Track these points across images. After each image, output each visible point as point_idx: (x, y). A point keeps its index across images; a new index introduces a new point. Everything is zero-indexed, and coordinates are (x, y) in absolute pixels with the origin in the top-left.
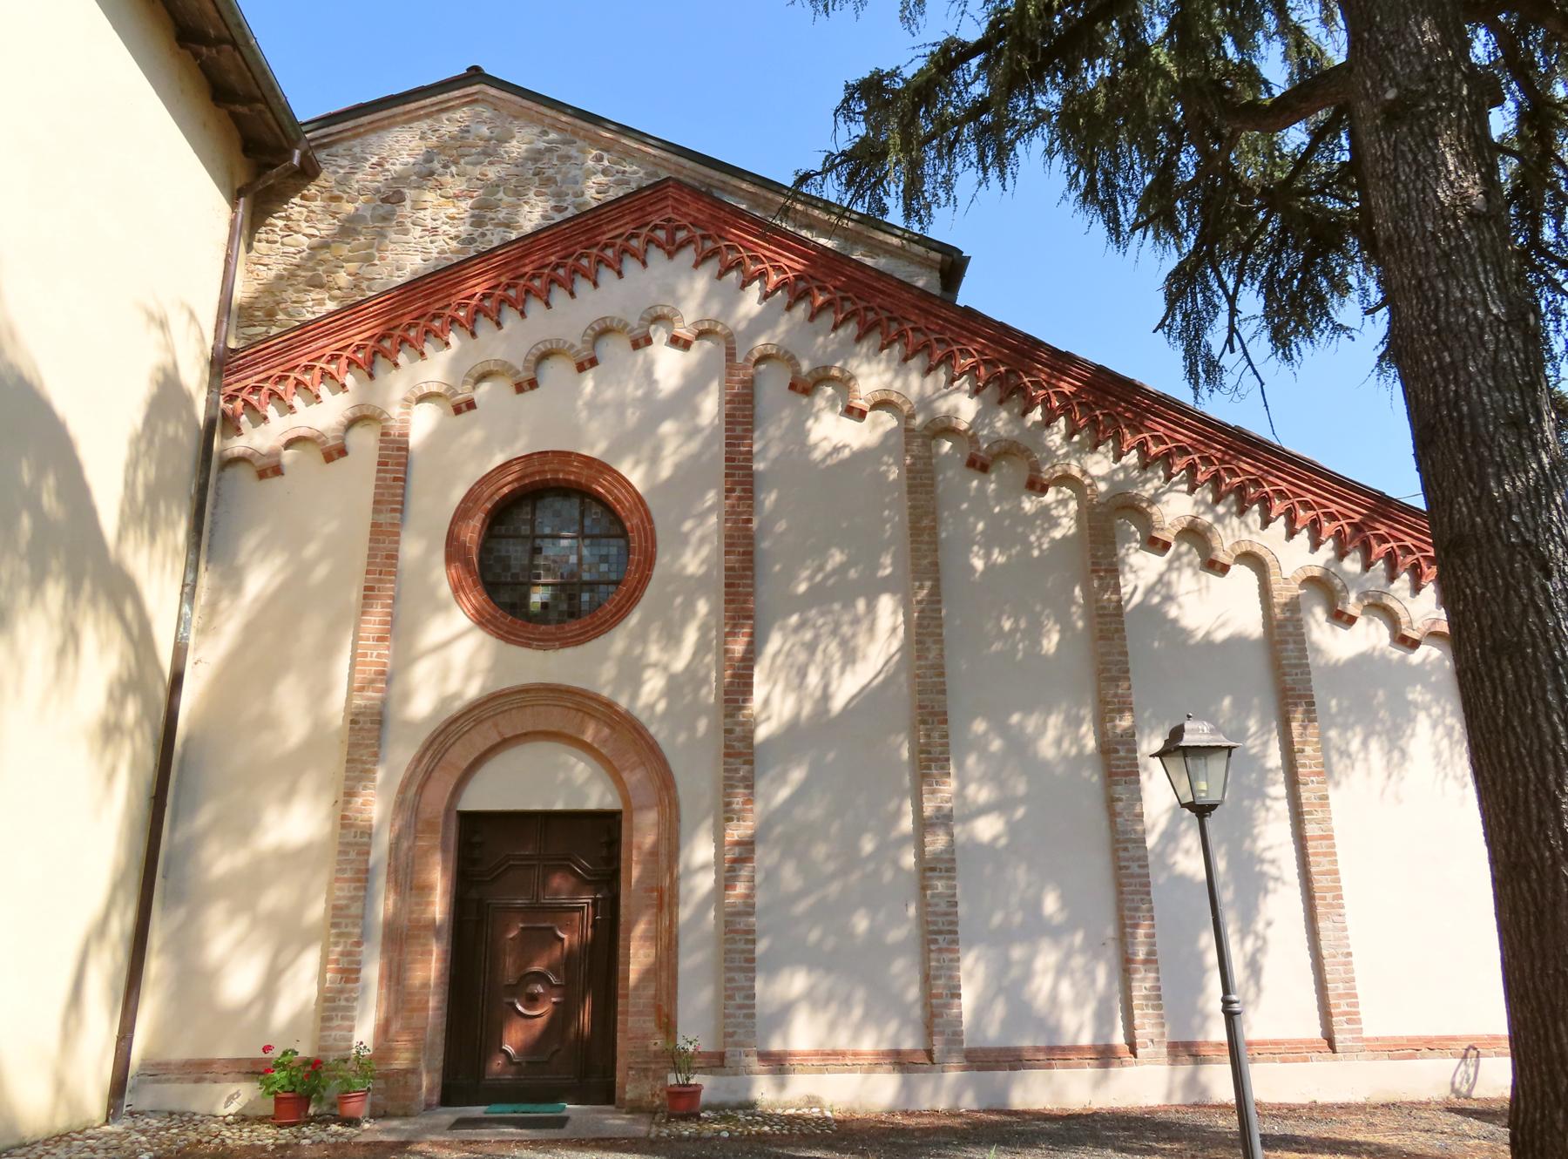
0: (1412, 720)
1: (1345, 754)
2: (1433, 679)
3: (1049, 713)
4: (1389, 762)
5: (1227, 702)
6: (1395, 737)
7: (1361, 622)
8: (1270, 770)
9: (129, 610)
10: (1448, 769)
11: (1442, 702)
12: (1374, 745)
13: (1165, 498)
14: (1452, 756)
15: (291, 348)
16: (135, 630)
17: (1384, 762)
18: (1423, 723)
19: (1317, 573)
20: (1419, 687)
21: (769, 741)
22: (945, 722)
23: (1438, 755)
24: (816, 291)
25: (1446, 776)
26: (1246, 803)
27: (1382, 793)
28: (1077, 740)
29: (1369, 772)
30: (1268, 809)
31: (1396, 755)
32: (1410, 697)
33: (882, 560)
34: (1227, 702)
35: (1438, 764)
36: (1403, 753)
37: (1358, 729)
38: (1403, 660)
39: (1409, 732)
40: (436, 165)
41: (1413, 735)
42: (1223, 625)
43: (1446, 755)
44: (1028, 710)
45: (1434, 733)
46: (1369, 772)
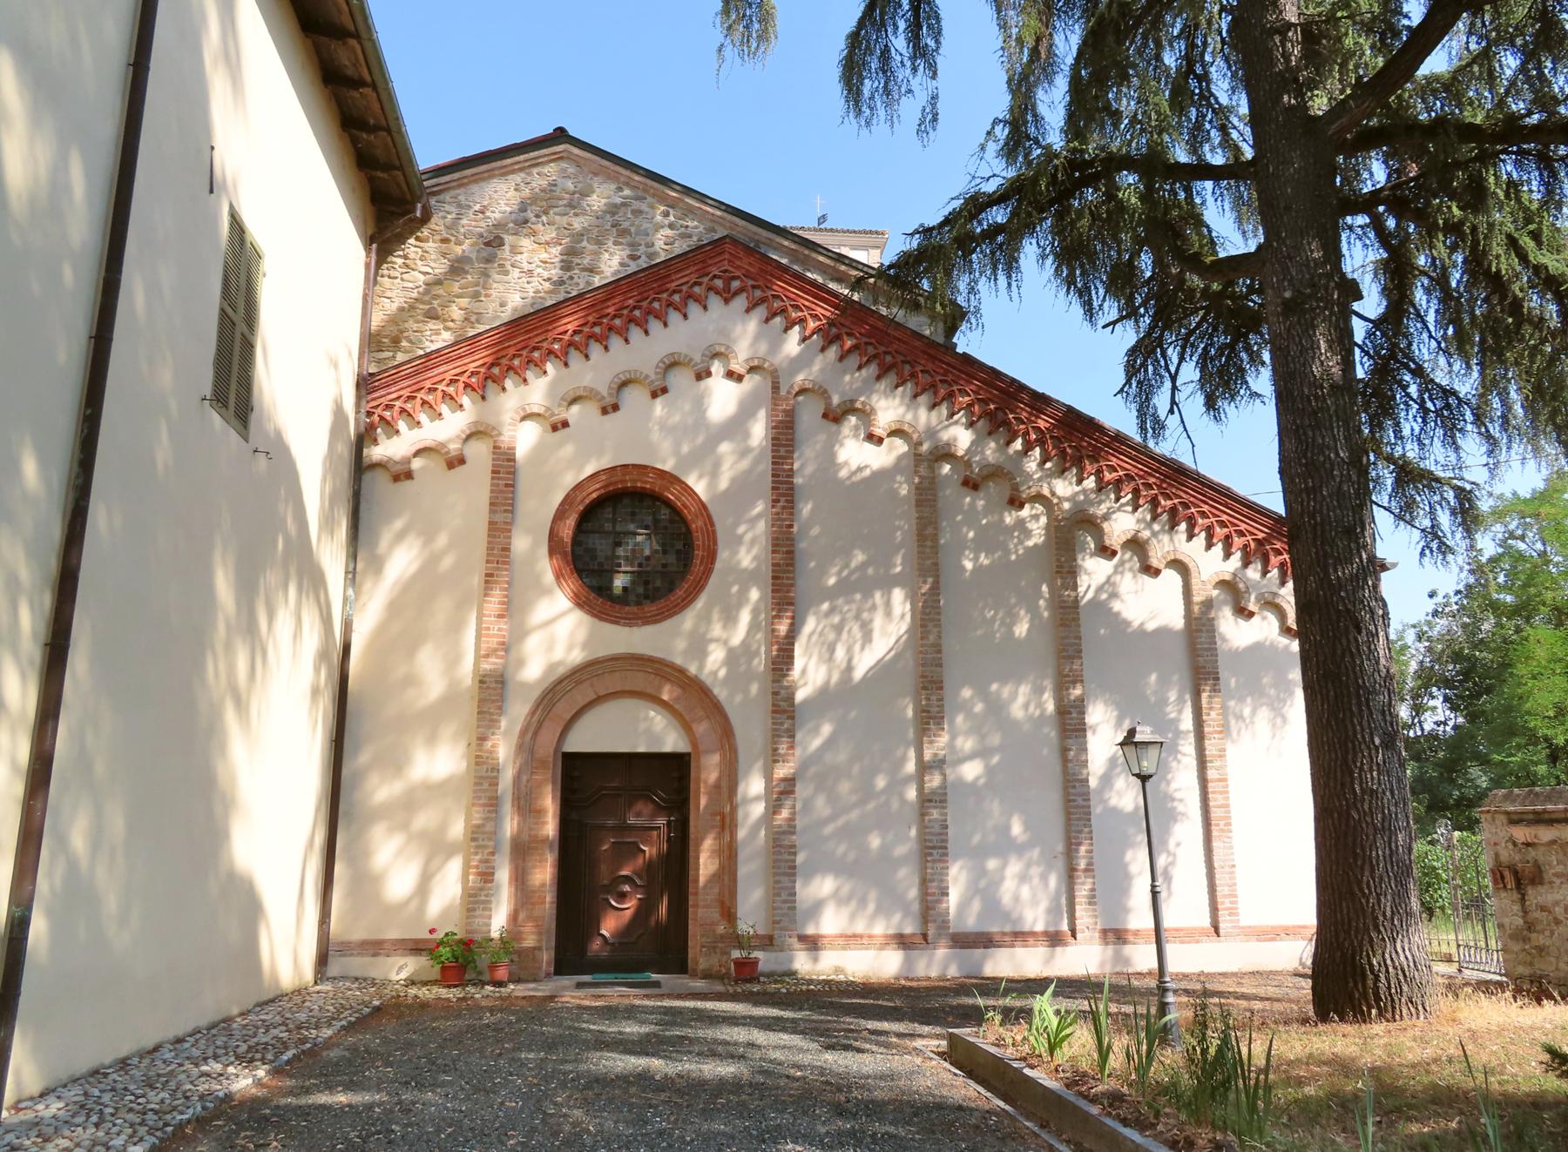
1: (1240, 717)
3: (1019, 684)
5: (1153, 677)
13: (1114, 516)
19: (1228, 577)
22: (941, 688)
28: (1040, 705)
34: (1153, 677)
36: (1284, 719)
41: (1291, 706)
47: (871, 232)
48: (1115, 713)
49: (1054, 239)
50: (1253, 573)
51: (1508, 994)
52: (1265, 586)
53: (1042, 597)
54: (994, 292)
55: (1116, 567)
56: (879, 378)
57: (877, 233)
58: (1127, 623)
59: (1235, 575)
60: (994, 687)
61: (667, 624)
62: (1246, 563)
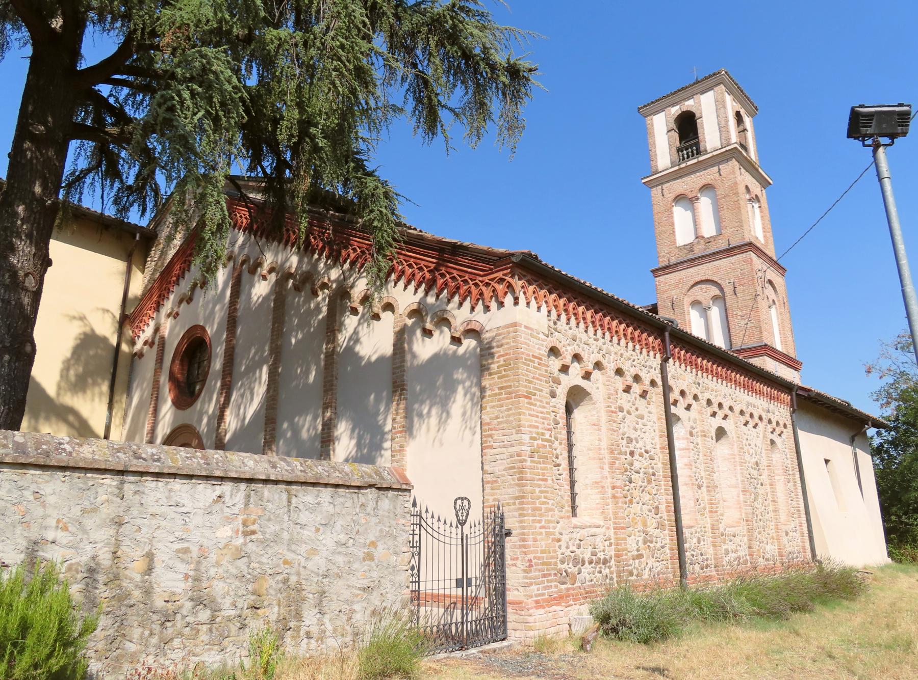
0: (454, 391)
1: (420, 415)
2: (469, 362)
3: (307, 415)
4: (440, 420)
5: (372, 397)
6: (444, 404)
7: (436, 334)
8: (386, 433)
9: (71, 418)
10: (468, 423)
11: (472, 377)
12: (434, 411)
13: (357, 283)
14: (471, 413)
15: (141, 310)
16: (77, 424)
17: (437, 421)
18: (460, 390)
19: (415, 307)
20: (460, 370)
21: (229, 441)
22: (275, 423)
23: (464, 414)
24: (789, 612)
25: (466, 427)
26: (374, 453)
27: (434, 441)
28: (315, 428)
29: (428, 430)
30: (382, 456)
31: (444, 415)
32: (455, 376)
33: (455, 376)
34: (372, 397)
35: (463, 420)
36: (448, 413)
37: (428, 402)
38: (455, 352)
39: (452, 399)
40: (641, 471)
41: (454, 402)
42: (375, 352)
43: (469, 413)
44: (300, 415)
45: (465, 399)
46: (428, 430)
47: (710, 76)
48: (351, 426)
49: (273, 162)
50: (431, 300)
51: (106, 329)
52: (438, 306)
53: (322, 352)
54: (140, 213)
55: (360, 320)
56: (279, 245)
57: (714, 74)
58: (361, 358)
59: (419, 303)
60: (296, 419)
61: (189, 410)
62: (427, 293)
